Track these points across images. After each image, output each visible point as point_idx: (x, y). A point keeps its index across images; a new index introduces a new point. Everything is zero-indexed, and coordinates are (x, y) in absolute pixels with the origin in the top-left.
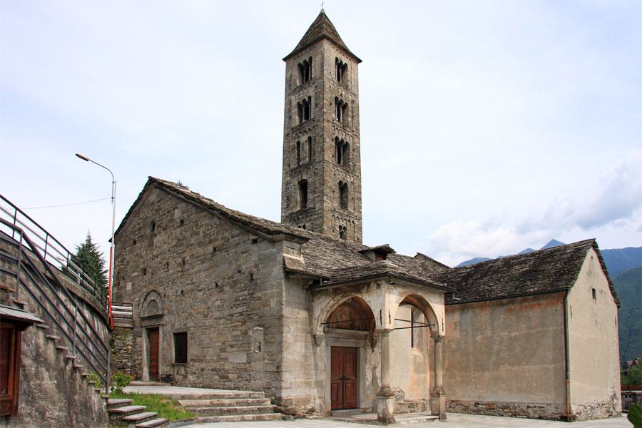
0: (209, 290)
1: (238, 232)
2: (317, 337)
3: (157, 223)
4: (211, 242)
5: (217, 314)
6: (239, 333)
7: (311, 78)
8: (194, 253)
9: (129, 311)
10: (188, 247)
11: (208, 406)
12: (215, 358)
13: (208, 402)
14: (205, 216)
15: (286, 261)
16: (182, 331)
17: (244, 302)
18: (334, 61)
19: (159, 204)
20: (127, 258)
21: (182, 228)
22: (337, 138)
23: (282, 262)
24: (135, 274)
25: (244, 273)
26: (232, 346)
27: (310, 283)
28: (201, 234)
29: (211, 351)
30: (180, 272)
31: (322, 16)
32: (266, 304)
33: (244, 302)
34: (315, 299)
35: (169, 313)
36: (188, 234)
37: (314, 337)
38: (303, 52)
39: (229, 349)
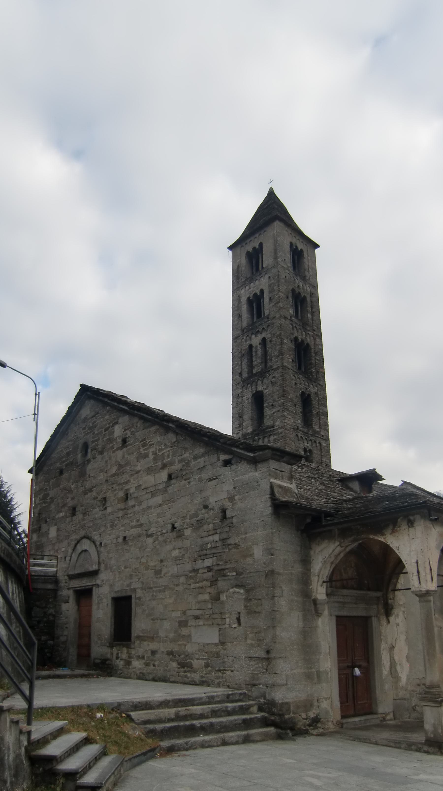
0: (162, 534)
1: (202, 450)
2: (318, 602)
3: (91, 446)
4: (164, 466)
5: (174, 570)
6: (207, 597)
7: (263, 267)
8: (141, 483)
9: (52, 566)
10: (132, 475)
11: (172, 720)
12: (171, 635)
13: (171, 712)
14: (155, 432)
15: (276, 490)
16: (124, 594)
17: (214, 551)
18: (288, 247)
19: (94, 419)
20: (52, 493)
21: (125, 449)
22: (296, 339)
23: (268, 491)
24: (62, 514)
25: (213, 509)
26: (197, 618)
27: (308, 520)
28: (151, 457)
29: (167, 625)
30: (122, 510)
31: (271, 195)
32: (248, 554)
33: (214, 551)
34: (314, 546)
35: (106, 568)
36: (132, 458)
37: (315, 602)
38: (252, 238)
39: (192, 622)
